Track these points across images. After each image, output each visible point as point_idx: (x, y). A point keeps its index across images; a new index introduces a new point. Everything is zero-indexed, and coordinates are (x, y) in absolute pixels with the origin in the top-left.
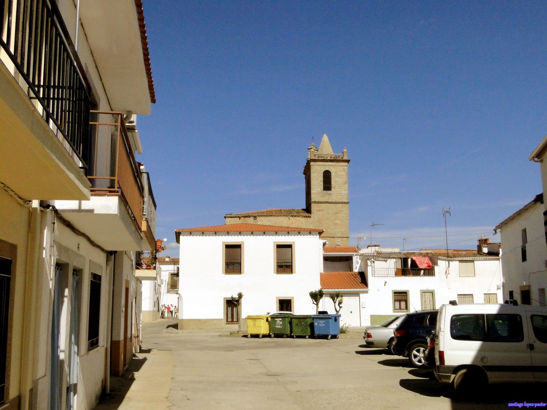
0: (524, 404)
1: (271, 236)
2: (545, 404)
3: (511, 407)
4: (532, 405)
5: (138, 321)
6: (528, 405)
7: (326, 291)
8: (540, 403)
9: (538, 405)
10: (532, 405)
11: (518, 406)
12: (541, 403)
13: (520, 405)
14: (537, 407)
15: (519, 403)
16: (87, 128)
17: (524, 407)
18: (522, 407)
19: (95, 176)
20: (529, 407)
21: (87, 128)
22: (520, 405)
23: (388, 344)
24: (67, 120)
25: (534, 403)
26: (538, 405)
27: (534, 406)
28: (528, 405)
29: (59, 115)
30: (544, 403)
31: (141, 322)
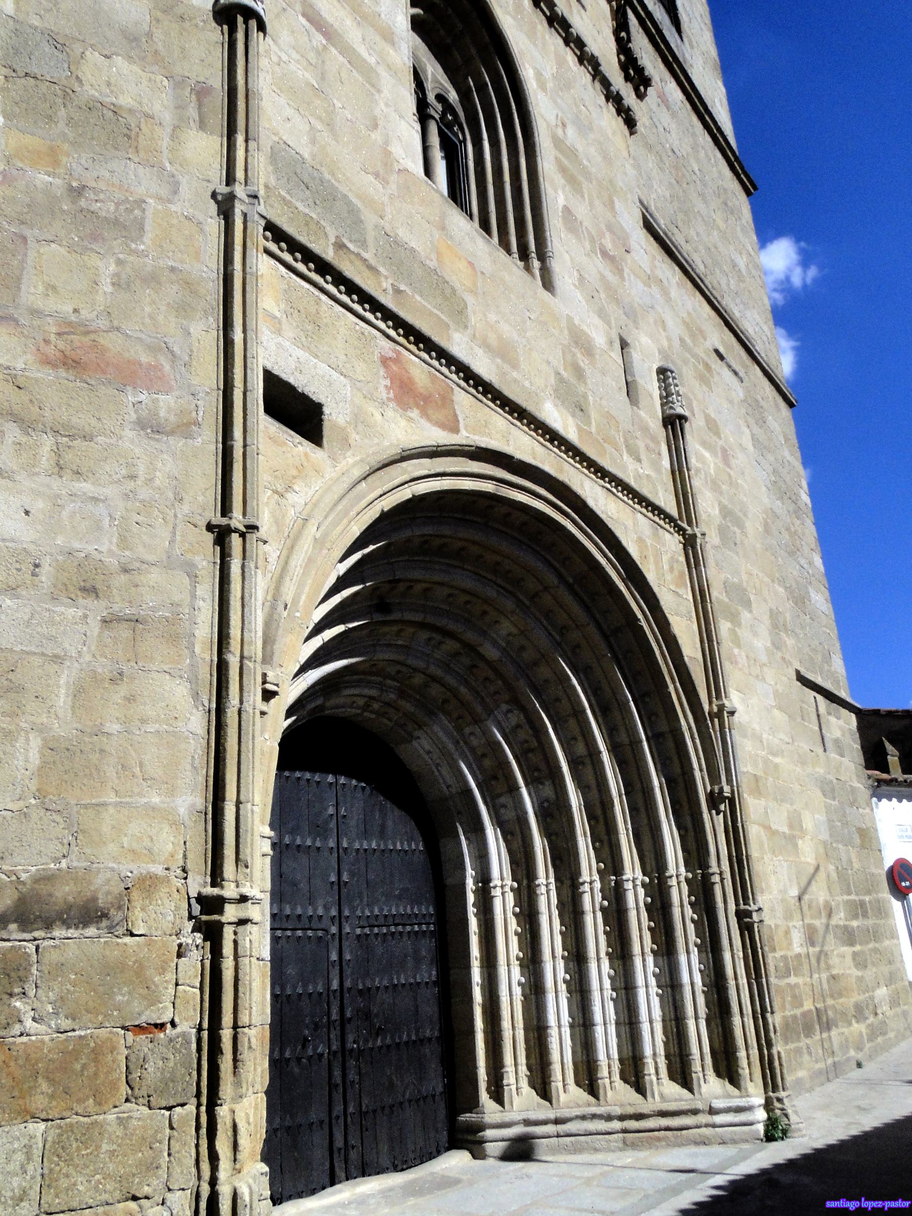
0: (860, 1202)
1: (900, 709)
2: (907, 1204)
3: (830, 1209)
4: (877, 1204)
5: (666, 1138)
6: (870, 1205)
7: (697, 961)
8: (896, 1200)
9: (893, 1204)
10: (877, 1204)
11: (848, 1208)
12: (897, 1200)
13: (852, 1205)
14: (889, 1208)
15: (850, 1200)
16: (632, 72)
17: (860, 1209)
18: (856, 1209)
19: (754, 904)
20: (873, 1208)
21: (632, 72)
22: (852, 1205)
23: (287, 717)
24: (653, 31)
25: (883, 1200)
26: (893, 1204)
27: (884, 1207)
28: (870, 1205)
29: (639, 8)
30: (904, 1200)
31: (342, 780)
